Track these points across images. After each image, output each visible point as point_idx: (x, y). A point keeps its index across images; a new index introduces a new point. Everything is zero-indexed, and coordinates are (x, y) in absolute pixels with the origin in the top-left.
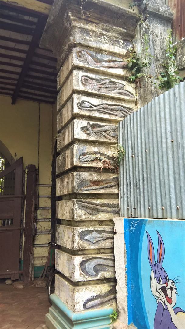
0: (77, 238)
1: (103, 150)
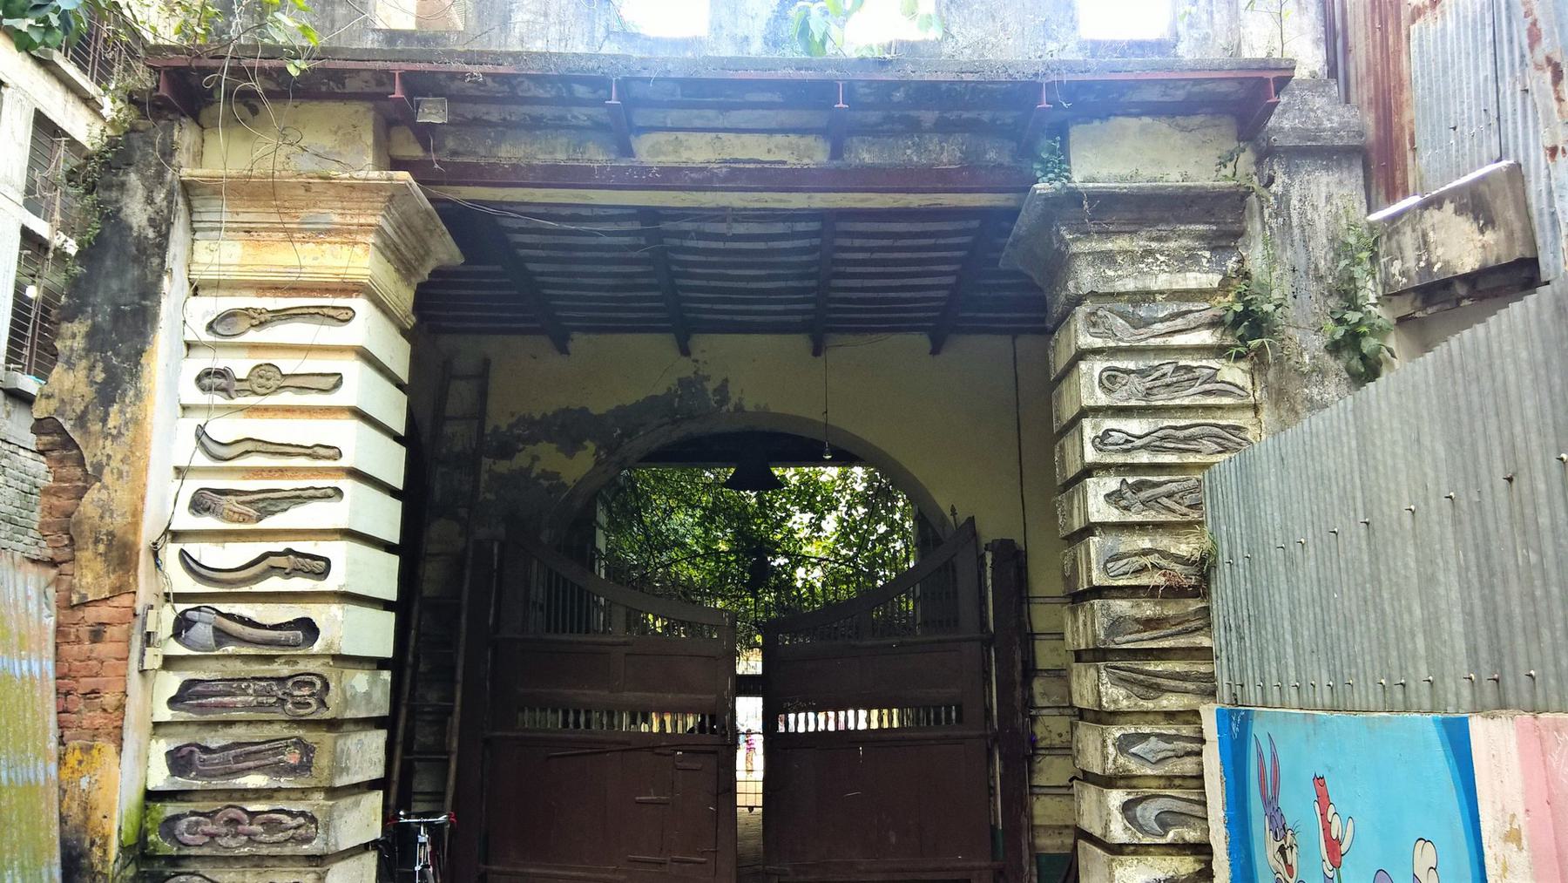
0: (1111, 750)
1: (1165, 542)
